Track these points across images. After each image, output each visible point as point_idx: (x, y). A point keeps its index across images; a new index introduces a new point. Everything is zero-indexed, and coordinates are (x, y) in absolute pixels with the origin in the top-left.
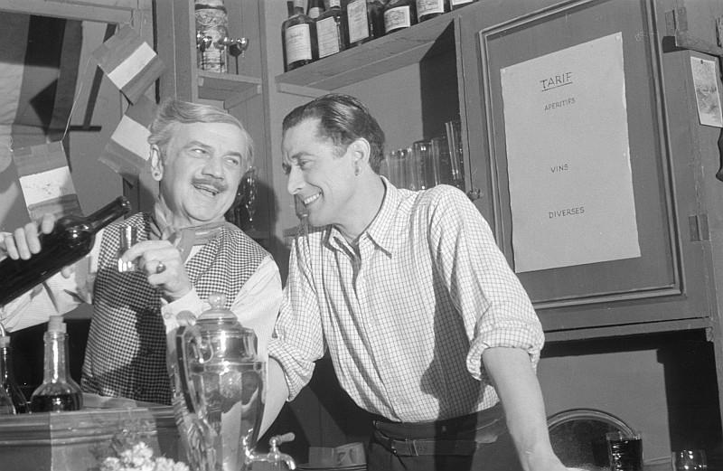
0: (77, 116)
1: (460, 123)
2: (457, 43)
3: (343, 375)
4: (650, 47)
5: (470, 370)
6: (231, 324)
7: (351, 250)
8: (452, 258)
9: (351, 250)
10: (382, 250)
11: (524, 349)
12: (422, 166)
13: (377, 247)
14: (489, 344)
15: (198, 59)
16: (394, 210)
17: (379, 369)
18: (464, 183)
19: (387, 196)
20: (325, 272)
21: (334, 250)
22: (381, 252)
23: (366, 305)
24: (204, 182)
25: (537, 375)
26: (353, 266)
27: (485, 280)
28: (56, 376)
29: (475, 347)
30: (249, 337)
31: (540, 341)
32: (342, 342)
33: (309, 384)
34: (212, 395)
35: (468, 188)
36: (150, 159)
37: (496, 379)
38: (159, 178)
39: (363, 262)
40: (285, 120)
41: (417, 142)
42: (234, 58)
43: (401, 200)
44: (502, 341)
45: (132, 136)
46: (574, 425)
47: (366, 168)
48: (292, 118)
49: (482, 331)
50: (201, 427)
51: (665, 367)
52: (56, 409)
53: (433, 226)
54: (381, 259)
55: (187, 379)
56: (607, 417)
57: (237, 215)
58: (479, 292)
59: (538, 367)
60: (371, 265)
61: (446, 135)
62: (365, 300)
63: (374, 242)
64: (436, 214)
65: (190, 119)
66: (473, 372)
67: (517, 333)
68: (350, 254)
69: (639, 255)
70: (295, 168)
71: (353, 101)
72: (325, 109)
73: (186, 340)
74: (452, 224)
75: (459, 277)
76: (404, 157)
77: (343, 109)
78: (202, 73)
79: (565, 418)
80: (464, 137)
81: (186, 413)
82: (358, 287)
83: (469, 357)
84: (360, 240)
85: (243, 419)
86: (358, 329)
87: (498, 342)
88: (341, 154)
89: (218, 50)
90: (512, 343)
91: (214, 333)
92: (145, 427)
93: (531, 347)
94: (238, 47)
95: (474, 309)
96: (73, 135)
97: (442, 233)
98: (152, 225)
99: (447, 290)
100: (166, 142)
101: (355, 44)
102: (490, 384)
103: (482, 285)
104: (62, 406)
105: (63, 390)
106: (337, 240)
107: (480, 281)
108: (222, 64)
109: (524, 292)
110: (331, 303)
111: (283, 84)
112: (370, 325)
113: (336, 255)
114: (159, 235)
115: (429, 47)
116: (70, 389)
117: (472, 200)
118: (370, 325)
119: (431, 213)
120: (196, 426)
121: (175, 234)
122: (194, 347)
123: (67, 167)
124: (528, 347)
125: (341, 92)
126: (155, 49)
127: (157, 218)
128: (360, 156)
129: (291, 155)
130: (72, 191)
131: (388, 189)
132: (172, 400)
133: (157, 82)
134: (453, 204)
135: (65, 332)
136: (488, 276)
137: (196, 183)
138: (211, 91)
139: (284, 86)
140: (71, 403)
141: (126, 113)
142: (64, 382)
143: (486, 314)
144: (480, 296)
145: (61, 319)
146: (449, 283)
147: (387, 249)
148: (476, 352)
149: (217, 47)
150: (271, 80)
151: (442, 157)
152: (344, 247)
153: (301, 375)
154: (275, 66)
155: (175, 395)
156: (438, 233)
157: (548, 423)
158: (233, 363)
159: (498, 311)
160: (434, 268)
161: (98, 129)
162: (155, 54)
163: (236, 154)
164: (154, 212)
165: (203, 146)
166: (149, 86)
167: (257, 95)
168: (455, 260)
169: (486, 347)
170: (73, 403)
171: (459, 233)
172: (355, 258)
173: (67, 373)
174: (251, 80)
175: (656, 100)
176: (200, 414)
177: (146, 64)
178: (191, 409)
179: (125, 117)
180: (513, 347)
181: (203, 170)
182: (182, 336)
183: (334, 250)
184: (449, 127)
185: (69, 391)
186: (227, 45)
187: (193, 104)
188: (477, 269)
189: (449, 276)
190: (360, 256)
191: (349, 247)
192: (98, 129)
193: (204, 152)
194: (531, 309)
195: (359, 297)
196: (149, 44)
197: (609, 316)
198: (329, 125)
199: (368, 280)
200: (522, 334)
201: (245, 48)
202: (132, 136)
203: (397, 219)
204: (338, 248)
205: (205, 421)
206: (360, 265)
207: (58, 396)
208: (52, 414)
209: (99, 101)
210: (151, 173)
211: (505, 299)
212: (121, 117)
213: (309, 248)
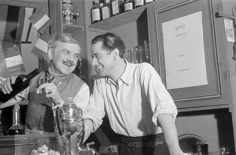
0: (23, 39)
1: (149, 41)
2: (148, 15)
3: (113, 124)
4: (211, 16)
5: (153, 122)
6: (74, 107)
7: (115, 84)
8: (148, 87)
9: (115, 84)
10: (125, 83)
11: (171, 115)
12: (137, 55)
13: (124, 83)
14: (160, 113)
15: (63, 20)
16: (129, 70)
17: (124, 122)
18: (150, 61)
19: (127, 66)
20: (107, 91)
21: (110, 84)
22: (125, 84)
23: (120, 102)
24: (66, 62)
25: (98, 128)
26: (116, 89)
27: (158, 93)
28: (17, 123)
29: (155, 114)
30: (80, 111)
31: (176, 113)
32: (113, 113)
33: (100, 127)
34: (68, 129)
35: (151, 62)
36: (48, 53)
37: (162, 125)
38: (51, 59)
39: (119, 88)
40: (92, 41)
41: (135, 47)
42: (75, 20)
43: (131, 67)
44: (164, 112)
45: (42, 45)
46: (186, 139)
47: (118, 58)
48: (94, 41)
49: (157, 109)
50: (64, 140)
51: (216, 117)
52: (17, 134)
53: (141, 76)
54: (125, 86)
55: (60, 125)
56: (197, 137)
57: (77, 72)
58: (156, 97)
59: (175, 121)
60: (122, 88)
61: (144, 45)
62: (120, 100)
63: (123, 81)
64: (142, 72)
65: (64, 41)
66: (154, 122)
67: (169, 110)
68: (115, 85)
69: (207, 84)
70: (95, 56)
71: (114, 35)
72: (104, 38)
73: (59, 111)
74: (147, 75)
75: (150, 92)
76: (131, 52)
77: (111, 39)
78: (64, 25)
79: (183, 137)
80: (150, 45)
81: (59, 135)
82: (117, 96)
83: (153, 118)
84: (118, 81)
85: (78, 137)
86: (117, 106)
87: (162, 112)
88: (110, 54)
89: (70, 17)
90: (167, 113)
91: (68, 109)
92: (45, 140)
93: (173, 114)
94: (76, 16)
95: (154, 102)
96: (22, 44)
97: (144, 78)
98: (47, 74)
99: (146, 96)
100: (55, 47)
101: (114, 15)
102: (160, 127)
103: (157, 94)
104: (19, 133)
105: (19, 128)
106: (110, 81)
107: (157, 93)
108: (71, 21)
109: (171, 97)
110: (109, 100)
111: (91, 28)
112: (121, 108)
113: (110, 85)
114: (49, 77)
115: (139, 17)
116: (21, 128)
117: (153, 66)
118: (121, 108)
119: (141, 71)
120: (62, 139)
121: (54, 77)
122: (62, 114)
123: (20, 55)
124: (172, 114)
125: (111, 31)
126: (49, 17)
127: (49, 72)
128: (116, 54)
129: (94, 53)
130: (22, 63)
131: (127, 64)
132: (55, 131)
133: (50, 27)
134: (148, 69)
135: (19, 109)
136: (159, 92)
137: (64, 62)
138: (68, 30)
139: (91, 29)
140: (22, 132)
141: (40, 38)
142: (19, 125)
143: (159, 104)
144: (157, 98)
145: (18, 105)
146: (147, 94)
147: (127, 83)
148: (155, 116)
149: (69, 16)
150: (87, 27)
151: (143, 52)
152: (113, 83)
153: (99, 122)
154: (88, 22)
155: (55, 130)
156: (143, 78)
157: (178, 138)
158: (75, 119)
159: (163, 103)
160: (141, 89)
161: (30, 43)
162: (49, 18)
163: (78, 54)
164: (48, 70)
165: (68, 51)
166: (47, 29)
167: (83, 31)
168: (148, 87)
169: (159, 114)
170: (22, 132)
171: (150, 78)
172: (117, 86)
173: (20, 123)
174: (80, 27)
175: (213, 34)
176: (64, 136)
177: (46, 21)
178: (61, 134)
179: (39, 39)
180: (168, 114)
181: (67, 58)
182: (58, 110)
183: (110, 84)
184: (145, 42)
185: (21, 128)
186: (73, 15)
187: (64, 36)
188: (155, 89)
189: (147, 92)
190: (118, 86)
191: (114, 83)
192: (30, 43)
193: (68, 52)
194: (173, 101)
195: (118, 99)
196: (47, 15)
197: (198, 104)
198: (106, 45)
199: (121, 94)
200: (170, 110)
201: (78, 17)
202: (42, 45)
203: (130, 73)
204: (111, 83)
205: (65, 138)
206: (118, 88)
207: (17, 130)
208: (15, 136)
209: (31, 33)
210: (48, 57)
211: (165, 99)
212: (38, 39)
213: (101, 84)
